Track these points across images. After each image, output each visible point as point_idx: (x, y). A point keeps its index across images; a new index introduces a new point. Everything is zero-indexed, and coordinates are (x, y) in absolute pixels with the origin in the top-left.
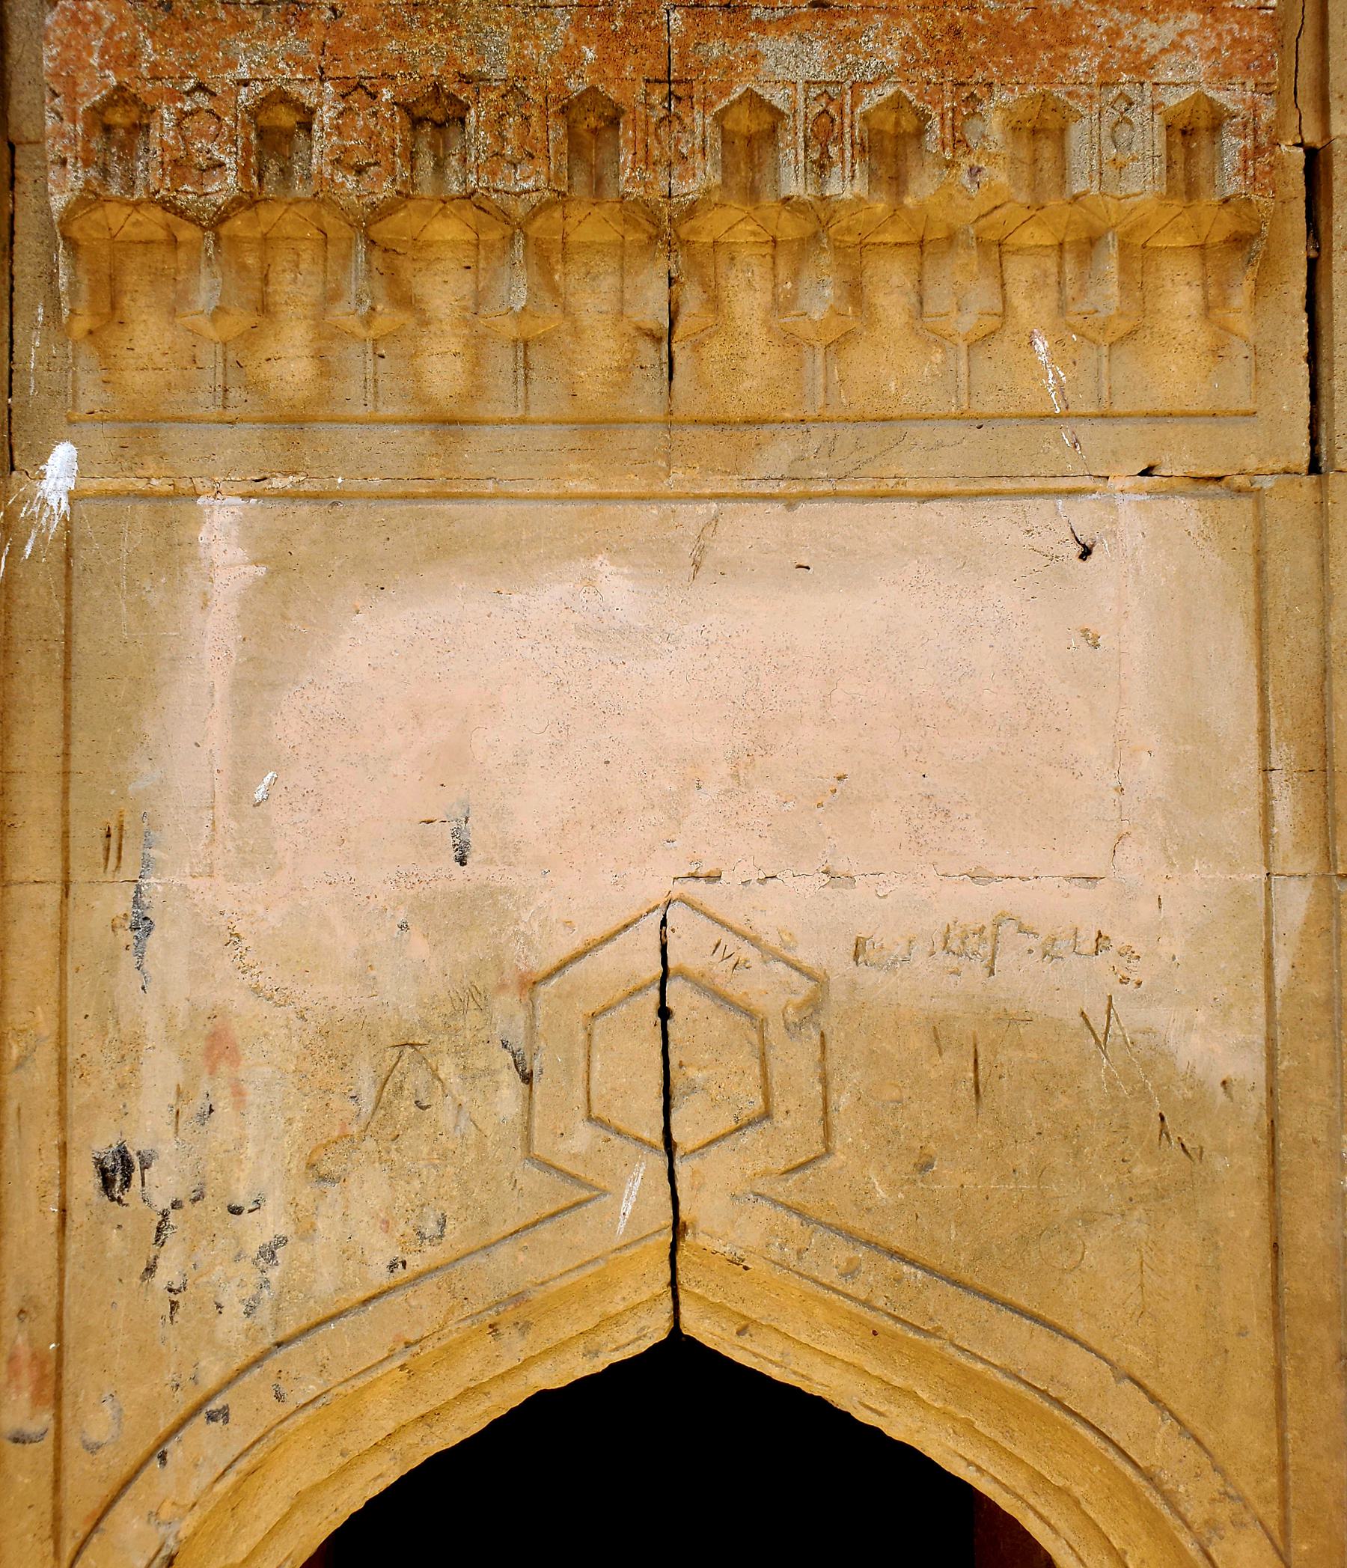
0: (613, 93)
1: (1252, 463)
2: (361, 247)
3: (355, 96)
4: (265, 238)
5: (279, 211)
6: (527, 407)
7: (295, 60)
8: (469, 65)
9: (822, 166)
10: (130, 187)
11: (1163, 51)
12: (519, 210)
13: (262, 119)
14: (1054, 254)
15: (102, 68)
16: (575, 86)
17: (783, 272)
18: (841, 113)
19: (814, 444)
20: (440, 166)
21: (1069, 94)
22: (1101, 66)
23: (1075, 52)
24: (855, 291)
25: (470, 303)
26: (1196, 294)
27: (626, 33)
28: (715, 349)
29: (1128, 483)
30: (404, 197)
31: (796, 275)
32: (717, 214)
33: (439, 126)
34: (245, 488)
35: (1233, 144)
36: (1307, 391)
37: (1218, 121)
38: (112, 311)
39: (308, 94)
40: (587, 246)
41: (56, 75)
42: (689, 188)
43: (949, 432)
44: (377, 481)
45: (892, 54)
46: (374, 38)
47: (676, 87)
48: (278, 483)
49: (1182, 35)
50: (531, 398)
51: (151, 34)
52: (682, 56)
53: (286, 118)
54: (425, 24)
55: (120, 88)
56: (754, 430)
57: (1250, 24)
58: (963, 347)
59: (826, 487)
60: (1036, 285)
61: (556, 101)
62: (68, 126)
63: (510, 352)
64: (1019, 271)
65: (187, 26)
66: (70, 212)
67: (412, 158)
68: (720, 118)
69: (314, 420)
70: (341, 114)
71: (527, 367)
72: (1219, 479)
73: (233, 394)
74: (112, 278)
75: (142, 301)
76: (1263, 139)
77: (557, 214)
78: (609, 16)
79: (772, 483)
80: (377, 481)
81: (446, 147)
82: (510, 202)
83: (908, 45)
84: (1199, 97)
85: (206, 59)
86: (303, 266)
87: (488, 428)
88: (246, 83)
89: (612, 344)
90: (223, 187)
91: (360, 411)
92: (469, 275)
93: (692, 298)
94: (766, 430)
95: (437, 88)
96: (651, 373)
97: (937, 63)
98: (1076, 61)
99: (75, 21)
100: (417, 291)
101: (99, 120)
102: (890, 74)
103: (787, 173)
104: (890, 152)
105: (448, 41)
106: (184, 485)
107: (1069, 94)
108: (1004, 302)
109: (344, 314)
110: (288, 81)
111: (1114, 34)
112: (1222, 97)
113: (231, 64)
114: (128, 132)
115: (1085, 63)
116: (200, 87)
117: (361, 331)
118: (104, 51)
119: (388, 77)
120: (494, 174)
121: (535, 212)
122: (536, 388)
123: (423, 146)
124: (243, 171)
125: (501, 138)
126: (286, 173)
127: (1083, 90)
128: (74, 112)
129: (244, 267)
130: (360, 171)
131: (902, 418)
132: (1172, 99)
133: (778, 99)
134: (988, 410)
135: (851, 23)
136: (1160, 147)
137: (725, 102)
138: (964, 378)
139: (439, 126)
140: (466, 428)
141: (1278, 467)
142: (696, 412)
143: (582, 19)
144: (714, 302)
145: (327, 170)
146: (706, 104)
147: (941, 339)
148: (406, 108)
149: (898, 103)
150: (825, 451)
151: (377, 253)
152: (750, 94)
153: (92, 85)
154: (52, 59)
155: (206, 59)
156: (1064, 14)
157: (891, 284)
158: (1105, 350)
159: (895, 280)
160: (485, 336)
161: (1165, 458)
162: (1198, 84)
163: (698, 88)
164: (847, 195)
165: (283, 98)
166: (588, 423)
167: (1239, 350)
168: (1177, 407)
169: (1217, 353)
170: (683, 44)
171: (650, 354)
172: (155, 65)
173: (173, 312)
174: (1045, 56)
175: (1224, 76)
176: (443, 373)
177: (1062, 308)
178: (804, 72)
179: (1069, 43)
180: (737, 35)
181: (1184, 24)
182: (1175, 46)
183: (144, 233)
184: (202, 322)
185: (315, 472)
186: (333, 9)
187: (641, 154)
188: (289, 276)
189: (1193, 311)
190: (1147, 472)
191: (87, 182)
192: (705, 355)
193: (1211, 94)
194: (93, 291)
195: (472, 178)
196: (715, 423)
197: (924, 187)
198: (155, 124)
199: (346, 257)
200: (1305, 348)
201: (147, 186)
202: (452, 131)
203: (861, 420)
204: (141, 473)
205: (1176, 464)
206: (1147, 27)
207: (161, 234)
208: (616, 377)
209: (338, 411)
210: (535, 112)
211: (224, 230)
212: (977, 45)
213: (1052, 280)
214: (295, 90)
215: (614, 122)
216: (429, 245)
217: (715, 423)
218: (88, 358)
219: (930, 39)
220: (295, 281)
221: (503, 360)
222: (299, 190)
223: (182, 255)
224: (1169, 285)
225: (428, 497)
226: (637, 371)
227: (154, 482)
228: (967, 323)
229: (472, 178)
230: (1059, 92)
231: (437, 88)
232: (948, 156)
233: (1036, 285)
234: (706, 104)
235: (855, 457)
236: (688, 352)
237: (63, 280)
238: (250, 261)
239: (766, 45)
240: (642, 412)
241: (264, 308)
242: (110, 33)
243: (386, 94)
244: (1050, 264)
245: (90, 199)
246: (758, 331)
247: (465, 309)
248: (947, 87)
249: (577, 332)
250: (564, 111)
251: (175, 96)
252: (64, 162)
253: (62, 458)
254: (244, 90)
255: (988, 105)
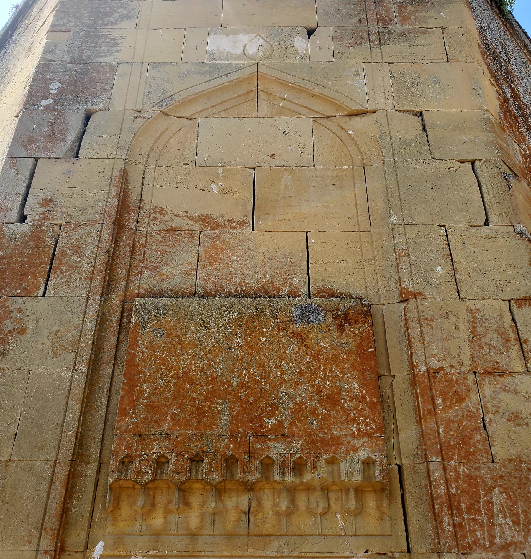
0: (237, 456)
1: (393, 550)
2: (177, 491)
3: (179, 456)
4: (155, 487)
5: (159, 481)
6: (213, 532)
7: (167, 448)
8: (205, 449)
9: (284, 473)
10: (126, 476)
11: (360, 446)
12: (215, 483)
13: (158, 460)
14: (340, 492)
15: (124, 450)
16: (228, 454)
17: (276, 497)
18: (288, 460)
19: (284, 542)
20: (197, 472)
21: (339, 456)
22: (346, 450)
23: (340, 446)
24: (293, 501)
25: (202, 504)
26: (375, 502)
27: (240, 441)
28: (260, 516)
29: (362, 555)
30: (188, 480)
31: (279, 498)
32: (260, 483)
33: (197, 461)
34: (143, 554)
35: (378, 469)
36: (404, 530)
37: (374, 462)
38: (117, 506)
39: (168, 456)
40: (230, 489)
41: (114, 451)
42: (253, 479)
43: (317, 539)
44: (176, 552)
45: (299, 447)
46: (184, 443)
47: (250, 454)
48: (151, 553)
49: (364, 443)
50: (215, 529)
51: (136, 442)
52: (252, 447)
53: (163, 460)
54: (196, 439)
55: (128, 454)
56: (269, 538)
57: (379, 440)
58: (319, 516)
59: (287, 555)
60: (337, 500)
61: (224, 457)
62: (115, 463)
63: (210, 517)
64: (332, 496)
65: (144, 440)
66: (112, 483)
67: (191, 470)
68: (261, 462)
69: (162, 535)
70: (176, 460)
71: (214, 520)
72: (385, 554)
73: (143, 527)
74: (118, 497)
75: (125, 503)
76: (384, 467)
77: (223, 483)
78: (236, 438)
79: (273, 553)
80: (176, 552)
81: (199, 467)
82: (212, 481)
83: (303, 444)
84: (369, 457)
85: (147, 447)
86: (163, 494)
87: (204, 537)
88: (155, 453)
89: (235, 514)
90: (148, 478)
91: (173, 532)
92: (202, 497)
93: (254, 504)
94: (273, 537)
95: (197, 454)
96: (244, 522)
97: (309, 449)
98: (340, 449)
99: (120, 439)
100: (189, 501)
101: (122, 462)
102: (299, 451)
103: (276, 474)
104: (299, 467)
105: (201, 443)
106: (129, 553)
107: (339, 456)
108: (329, 504)
109: (172, 507)
110: (165, 453)
111: (349, 442)
112: (374, 457)
113: (153, 449)
114: (128, 463)
115: (343, 449)
116: (145, 454)
117: (176, 512)
118: (126, 446)
119: (187, 452)
120: (209, 475)
121: (218, 483)
122: (216, 526)
123: (194, 467)
124: (153, 474)
125: (211, 466)
126: (162, 473)
127: (343, 455)
128: (117, 460)
129: (150, 495)
130: (179, 473)
131: (305, 535)
132: (363, 457)
133: (273, 457)
134: (326, 533)
135: (290, 439)
136: (361, 469)
137: (262, 458)
138: (320, 525)
139: (197, 461)
140: (198, 537)
141: (399, 551)
142: (255, 533)
143: (230, 438)
144: (260, 504)
145: (172, 474)
146: (257, 459)
147: (314, 514)
148: (190, 459)
149: (301, 458)
150: (286, 544)
151: (181, 492)
152: (267, 456)
153: (122, 453)
154: (114, 448)
155: (147, 447)
156: (337, 437)
157: (302, 499)
158: (353, 518)
159: (303, 498)
160: (205, 512)
161: (371, 548)
162: (368, 454)
163: (256, 455)
164: (289, 481)
165: (163, 456)
166: (229, 535)
167: (387, 518)
168: (373, 533)
169: (381, 518)
170: (253, 444)
171: (244, 517)
172: (136, 449)
173: (132, 506)
174: (334, 447)
175: (374, 453)
176: (194, 522)
177: (342, 507)
178: (280, 451)
179: (339, 444)
180: (265, 442)
181: (364, 440)
182: (362, 445)
183: (127, 486)
184: (139, 509)
185: (161, 550)
186: (176, 436)
187: (242, 470)
188: (160, 497)
189: (375, 507)
190: (366, 552)
191: (118, 476)
192: (257, 517)
193: (371, 456)
194: (114, 501)
195: (204, 476)
196: (259, 536)
197: (308, 477)
198: (134, 462)
199: (174, 492)
200: (403, 517)
201: (130, 477)
202: (200, 463)
203: (295, 535)
204: (118, 550)
205: (374, 549)
206: (356, 441)
207: (131, 486)
208: (235, 523)
209: (168, 533)
210: (219, 460)
211: (146, 486)
212: (318, 445)
213: (340, 499)
214: (165, 454)
215: (237, 461)
216: (193, 489)
217: (259, 536)
218: (110, 518)
219: (307, 443)
220: (161, 498)
221: (208, 519)
222: (164, 477)
223: (136, 491)
224: (368, 500)
225: (187, 556)
226: (241, 522)
227: (121, 552)
228: (320, 510)
229: (204, 476)
230: (337, 456)
231: (197, 454)
232: (312, 471)
233: (337, 500)
234: (257, 459)
235: (294, 546)
236: (253, 517)
237: (108, 499)
238: (151, 493)
239: (271, 444)
240: (242, 533)
241: (153, 505)
242: (127, 442)
243: (186, 456)
244: (339, 494)
245: (118, 479)
246: (270, 512)
247: (200, 505)
248: (312, 454)
249: (227, 511)
250: (225, 460)
251: (139, 456)
252: (113, 472)
253: (100, 545)
254: (155, 455)
255: (321, 459)
